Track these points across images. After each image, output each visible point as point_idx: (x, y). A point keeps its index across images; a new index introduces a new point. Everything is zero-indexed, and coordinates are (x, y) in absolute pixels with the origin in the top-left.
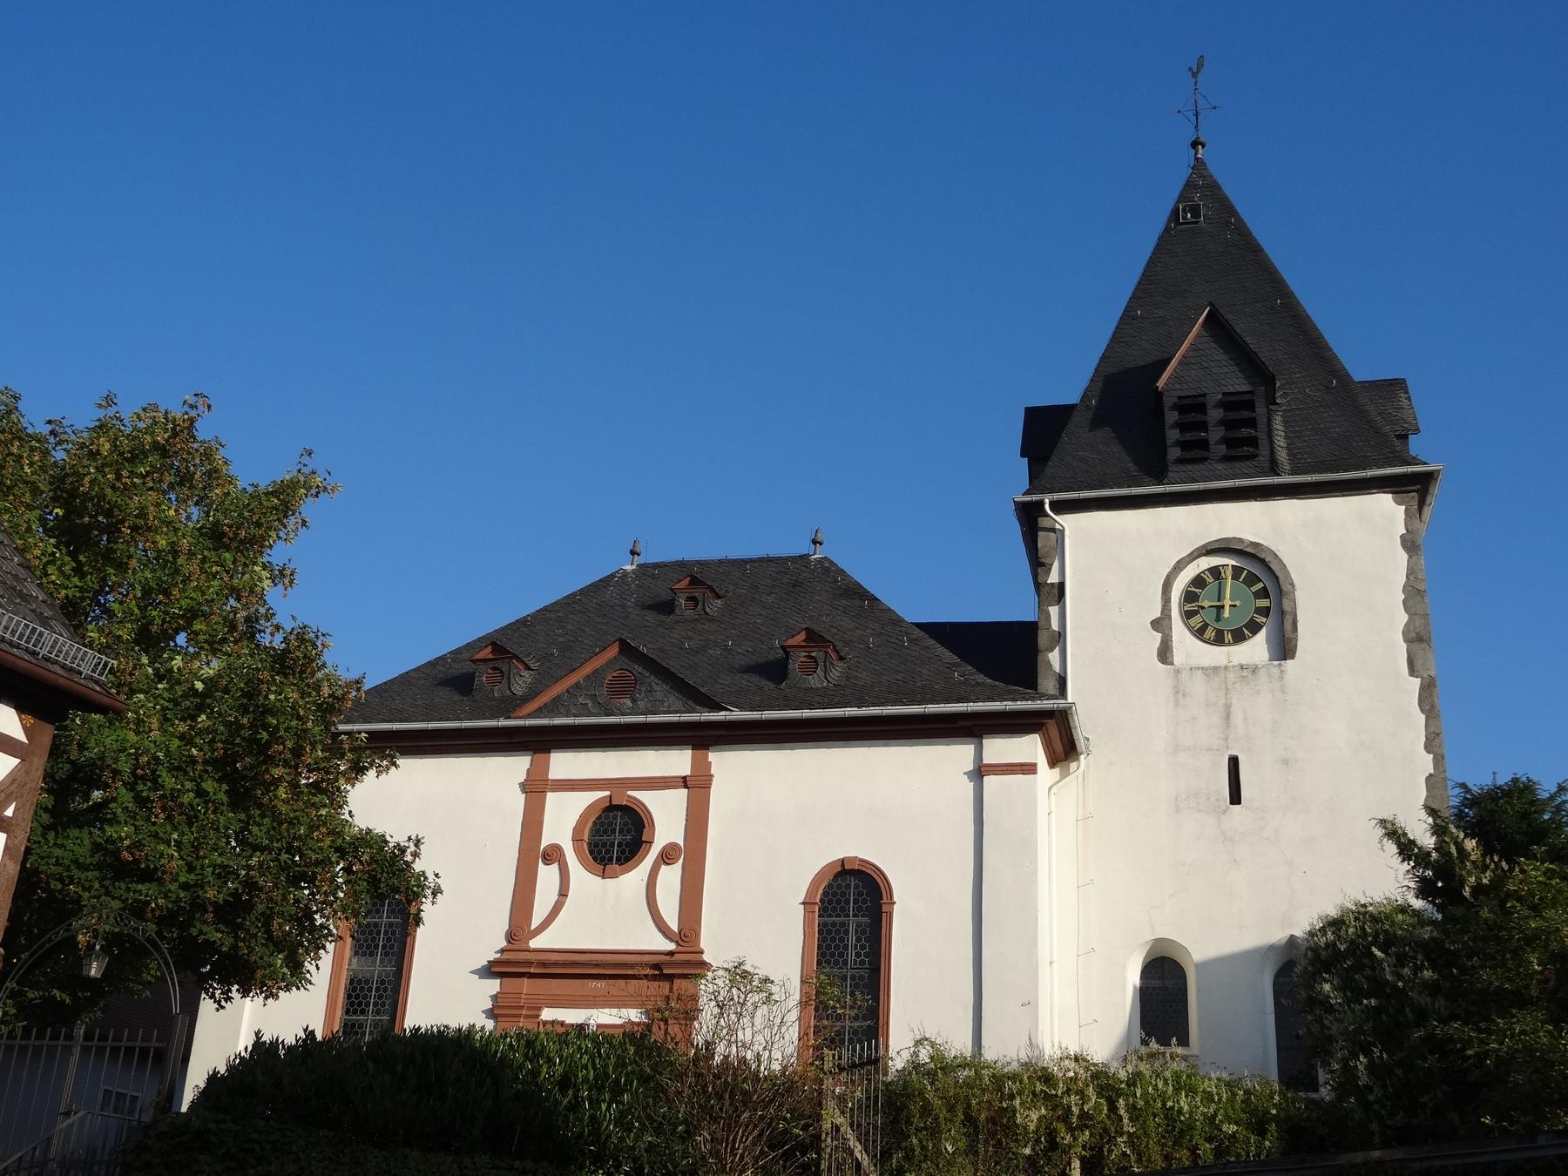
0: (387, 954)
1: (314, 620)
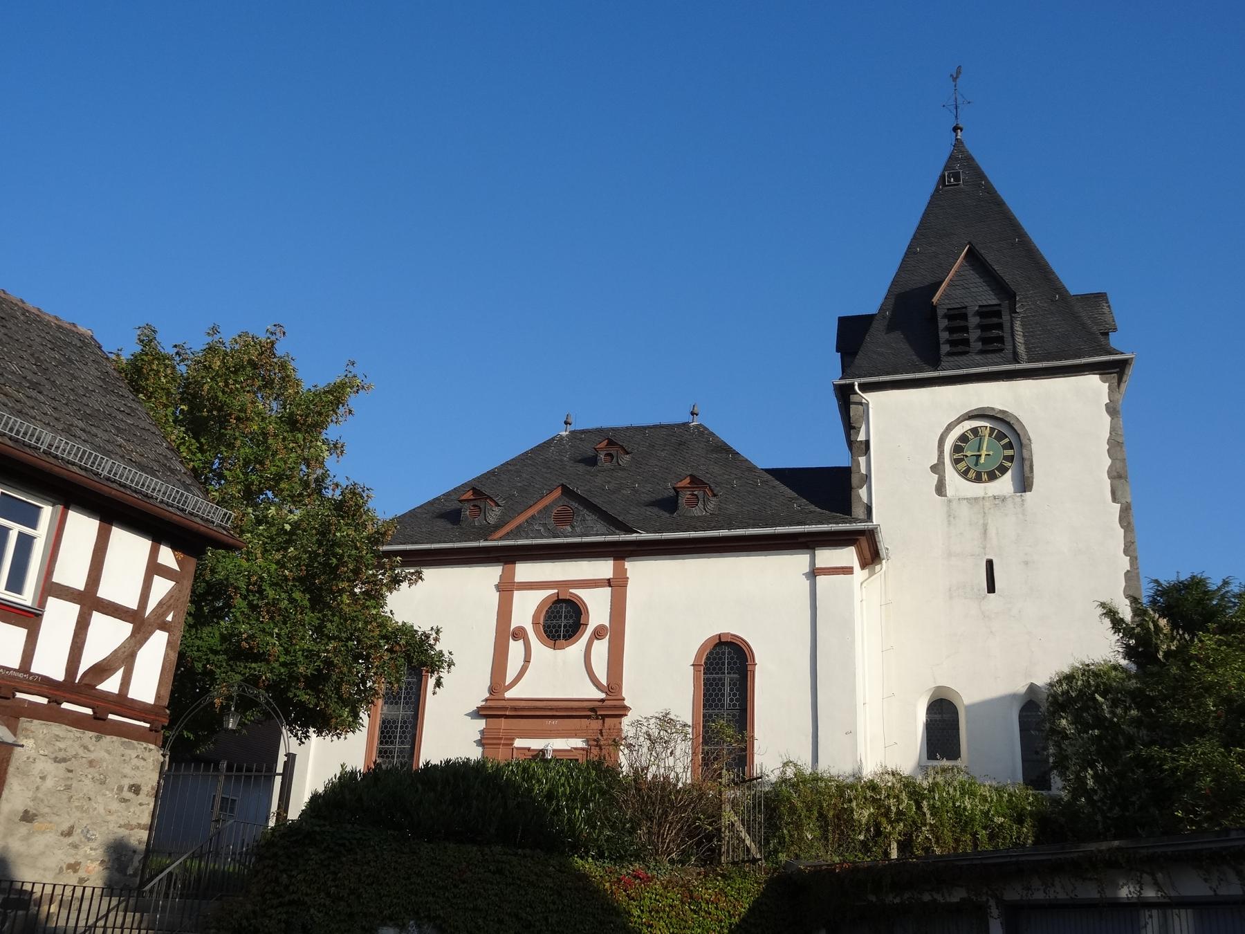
1: (361, 480)
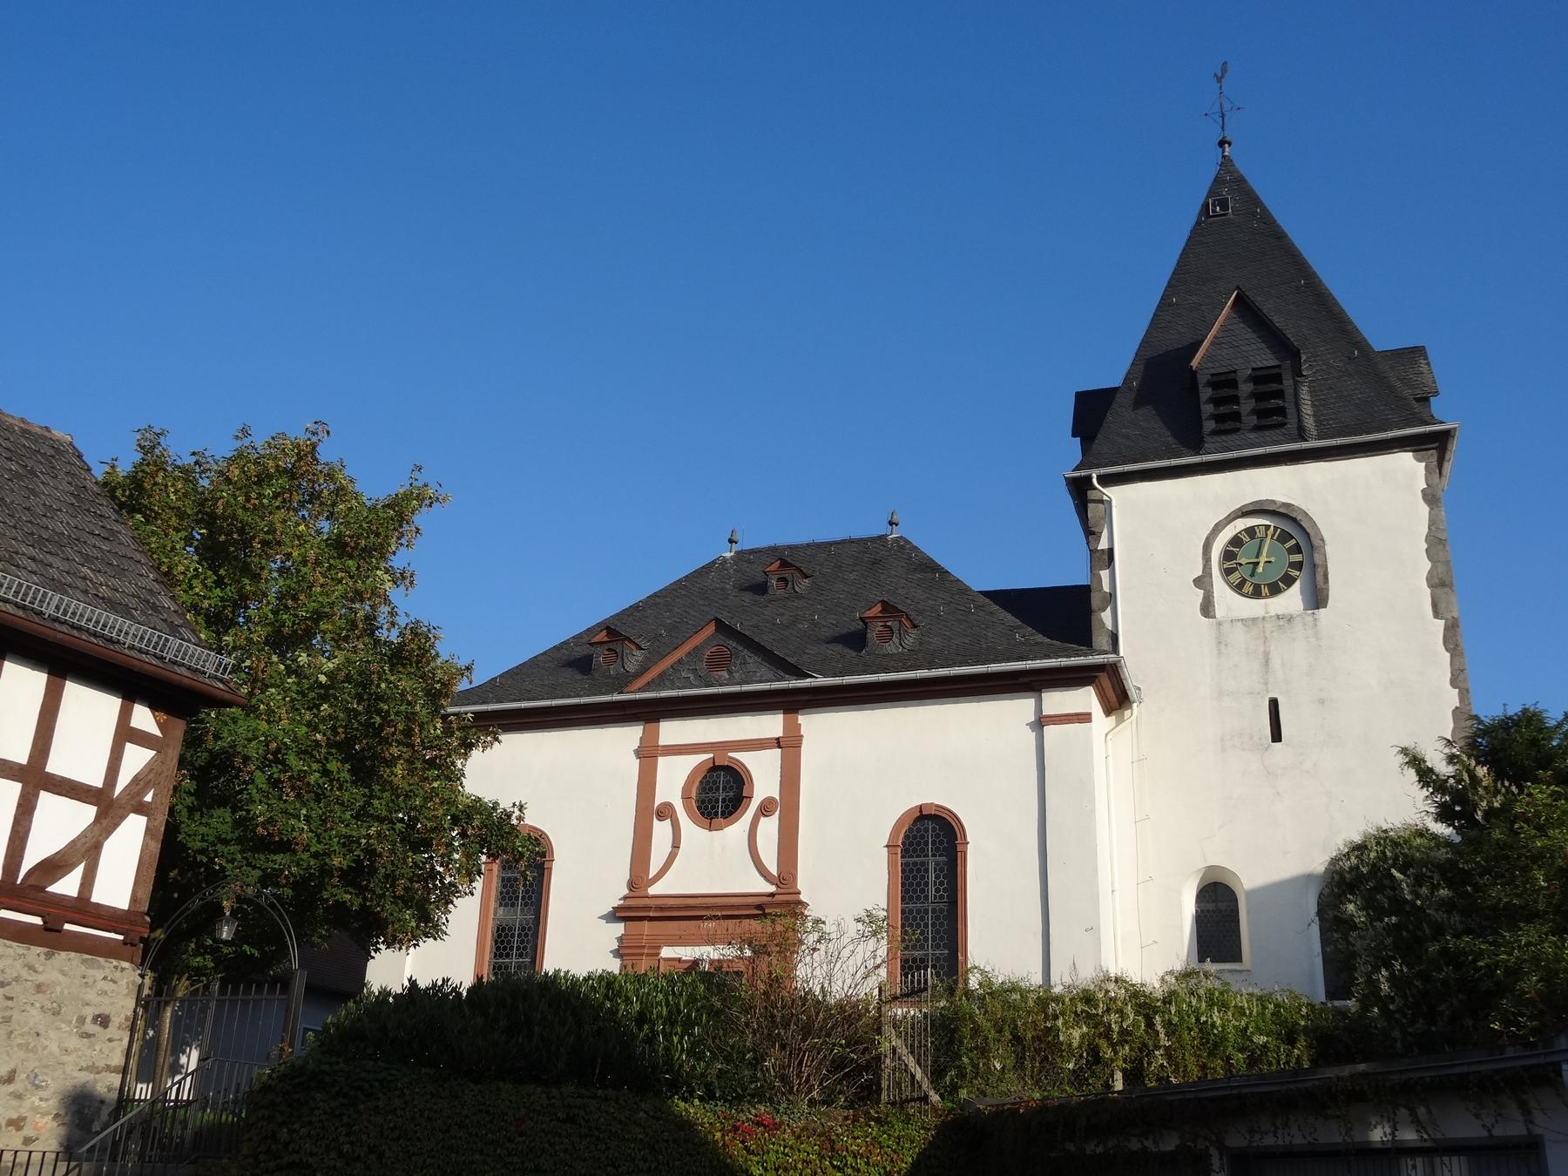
0: (526, 905)
